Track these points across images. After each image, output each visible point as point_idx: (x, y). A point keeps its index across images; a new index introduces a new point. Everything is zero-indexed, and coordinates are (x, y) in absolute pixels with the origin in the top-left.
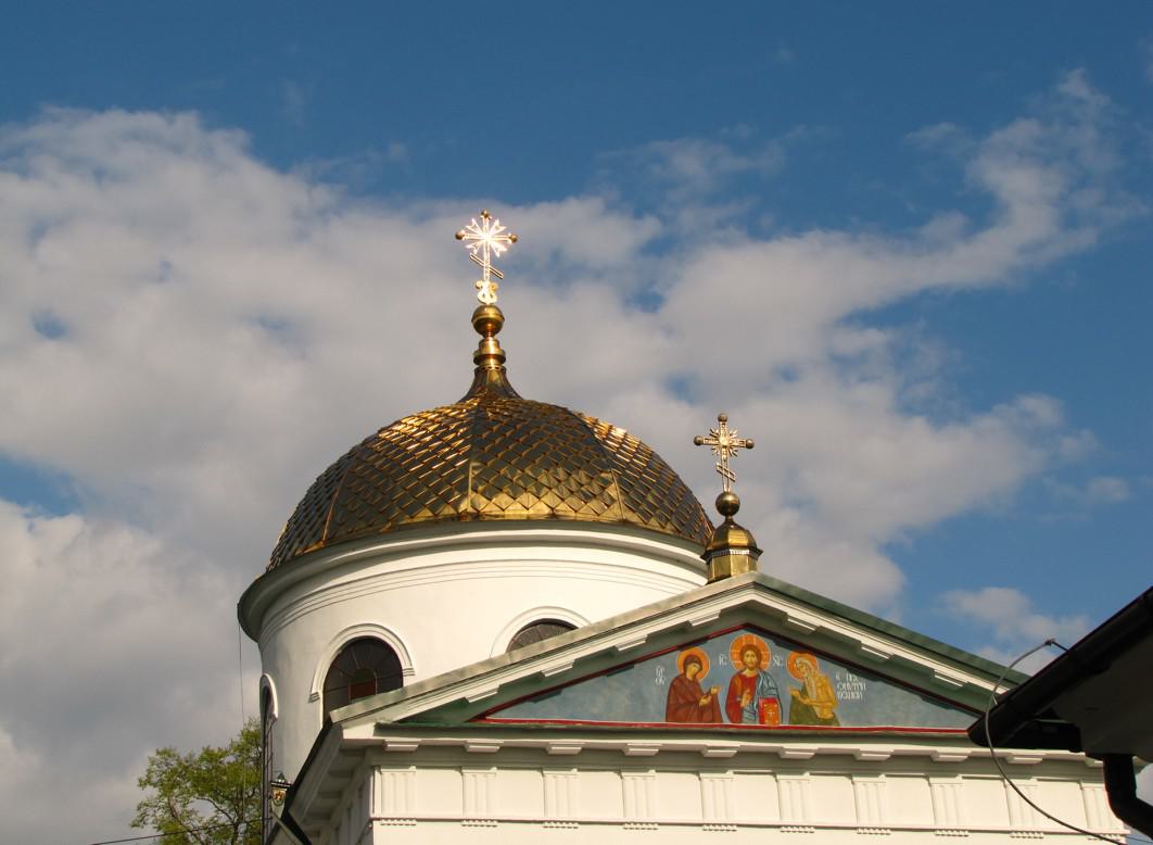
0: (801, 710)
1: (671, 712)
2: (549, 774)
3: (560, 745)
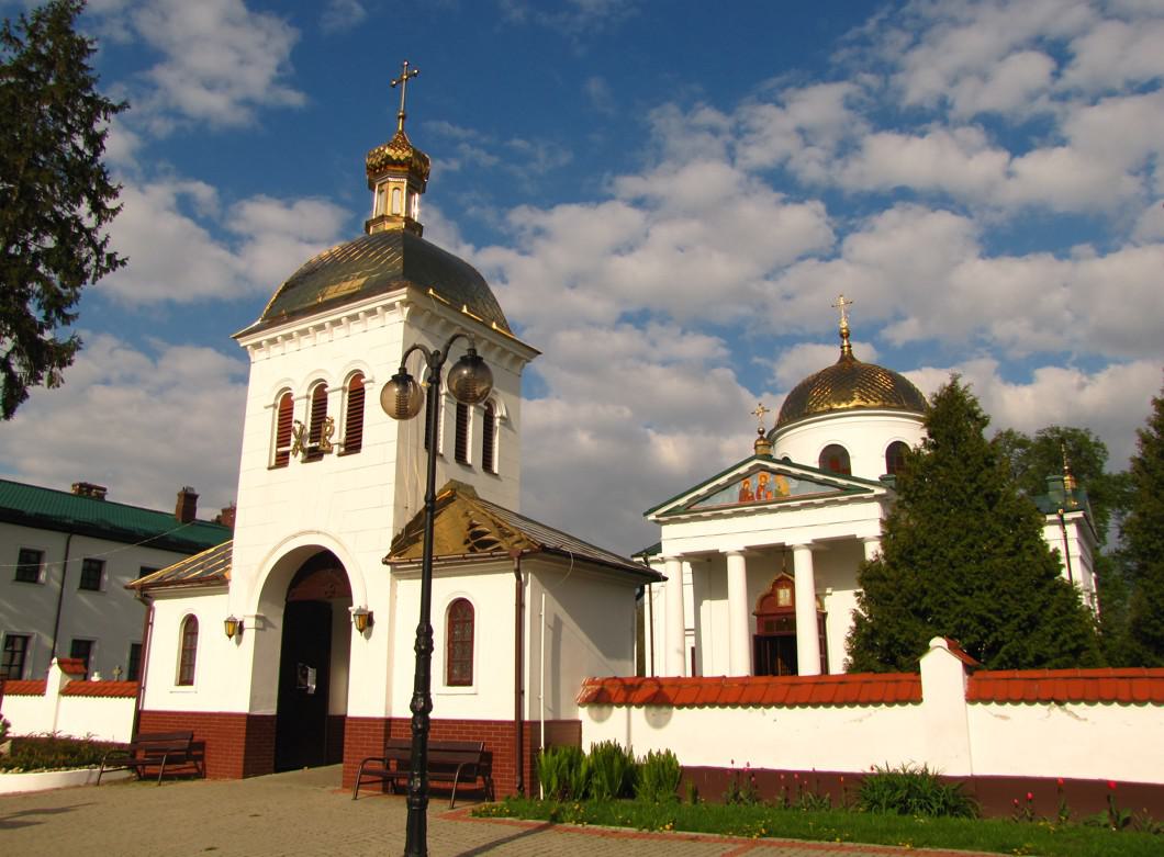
0: (778, 494)
1: (741, 500)
2: (969, 775)
3: (704, 514)
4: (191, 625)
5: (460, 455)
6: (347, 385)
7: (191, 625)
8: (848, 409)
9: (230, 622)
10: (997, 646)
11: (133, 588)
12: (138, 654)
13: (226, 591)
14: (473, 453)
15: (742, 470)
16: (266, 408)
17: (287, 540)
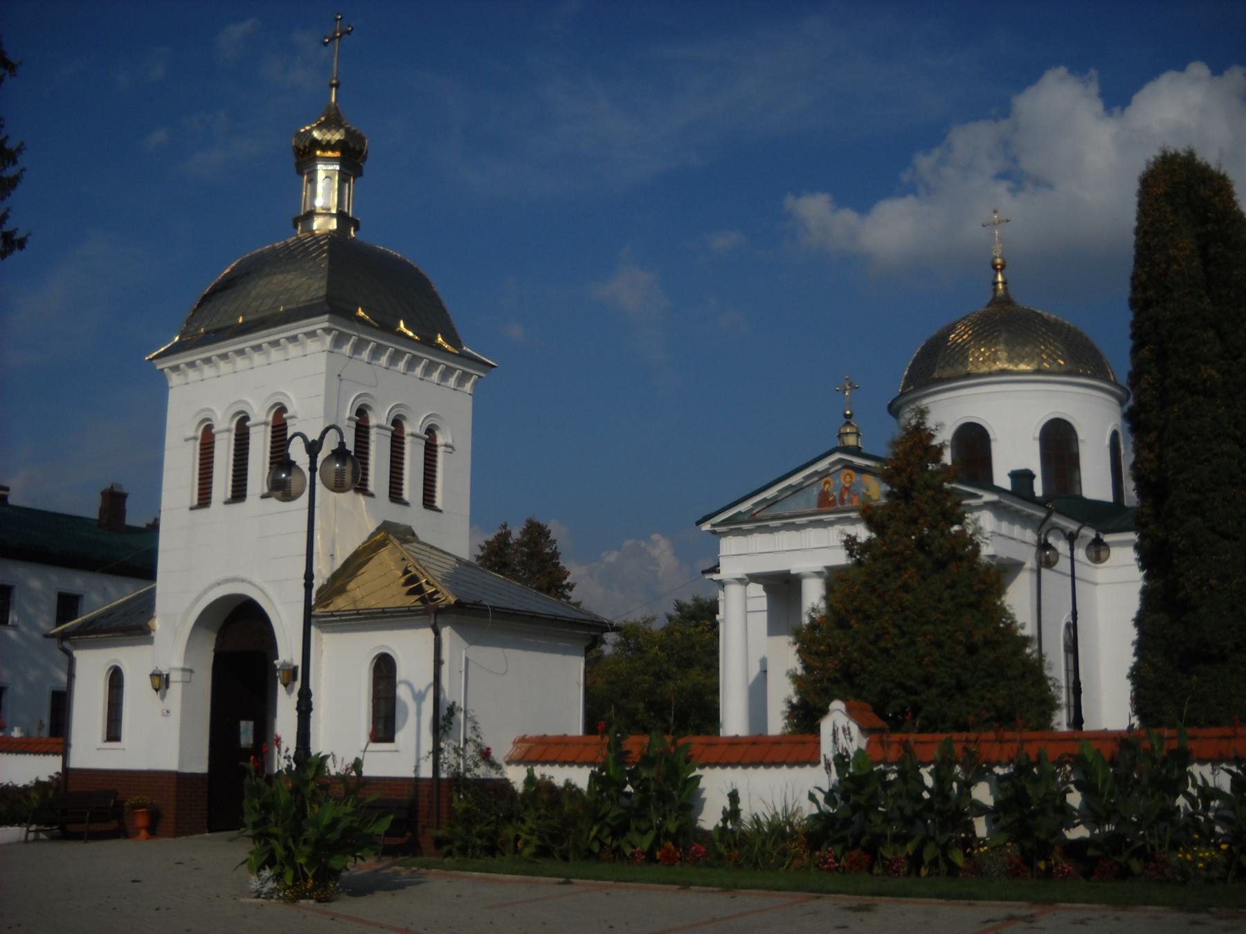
1: (820, 504)
4: (116, 679)
5: (395, 494)
6: (270, 418)
7: (116, 679)
8: (990, 374)
9: (156, 676)
10: (916, 710)
11: (53, 636)
12: (61, 703)
13: (150, 641)
14: (412, 486)
15: (770, 493)
16: (186, 440)
17: (205, 592)
